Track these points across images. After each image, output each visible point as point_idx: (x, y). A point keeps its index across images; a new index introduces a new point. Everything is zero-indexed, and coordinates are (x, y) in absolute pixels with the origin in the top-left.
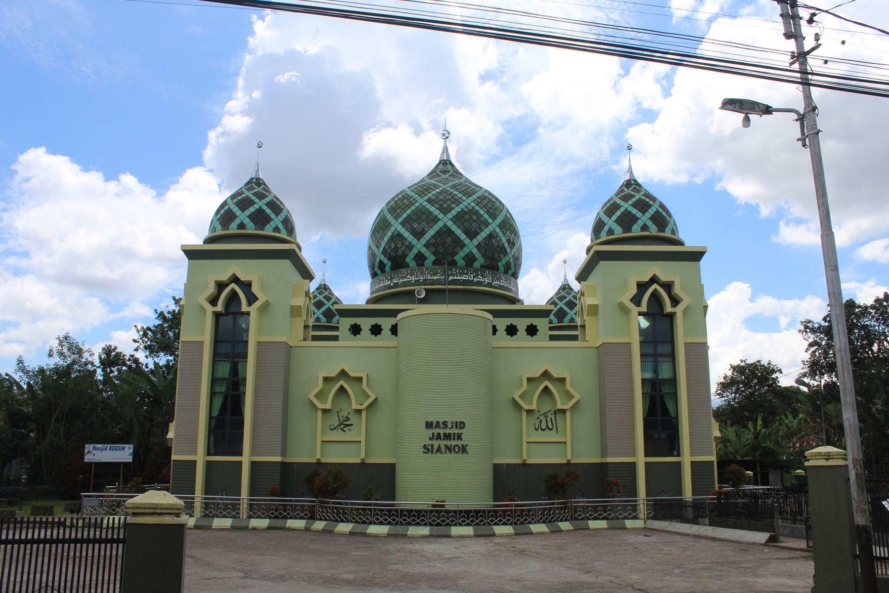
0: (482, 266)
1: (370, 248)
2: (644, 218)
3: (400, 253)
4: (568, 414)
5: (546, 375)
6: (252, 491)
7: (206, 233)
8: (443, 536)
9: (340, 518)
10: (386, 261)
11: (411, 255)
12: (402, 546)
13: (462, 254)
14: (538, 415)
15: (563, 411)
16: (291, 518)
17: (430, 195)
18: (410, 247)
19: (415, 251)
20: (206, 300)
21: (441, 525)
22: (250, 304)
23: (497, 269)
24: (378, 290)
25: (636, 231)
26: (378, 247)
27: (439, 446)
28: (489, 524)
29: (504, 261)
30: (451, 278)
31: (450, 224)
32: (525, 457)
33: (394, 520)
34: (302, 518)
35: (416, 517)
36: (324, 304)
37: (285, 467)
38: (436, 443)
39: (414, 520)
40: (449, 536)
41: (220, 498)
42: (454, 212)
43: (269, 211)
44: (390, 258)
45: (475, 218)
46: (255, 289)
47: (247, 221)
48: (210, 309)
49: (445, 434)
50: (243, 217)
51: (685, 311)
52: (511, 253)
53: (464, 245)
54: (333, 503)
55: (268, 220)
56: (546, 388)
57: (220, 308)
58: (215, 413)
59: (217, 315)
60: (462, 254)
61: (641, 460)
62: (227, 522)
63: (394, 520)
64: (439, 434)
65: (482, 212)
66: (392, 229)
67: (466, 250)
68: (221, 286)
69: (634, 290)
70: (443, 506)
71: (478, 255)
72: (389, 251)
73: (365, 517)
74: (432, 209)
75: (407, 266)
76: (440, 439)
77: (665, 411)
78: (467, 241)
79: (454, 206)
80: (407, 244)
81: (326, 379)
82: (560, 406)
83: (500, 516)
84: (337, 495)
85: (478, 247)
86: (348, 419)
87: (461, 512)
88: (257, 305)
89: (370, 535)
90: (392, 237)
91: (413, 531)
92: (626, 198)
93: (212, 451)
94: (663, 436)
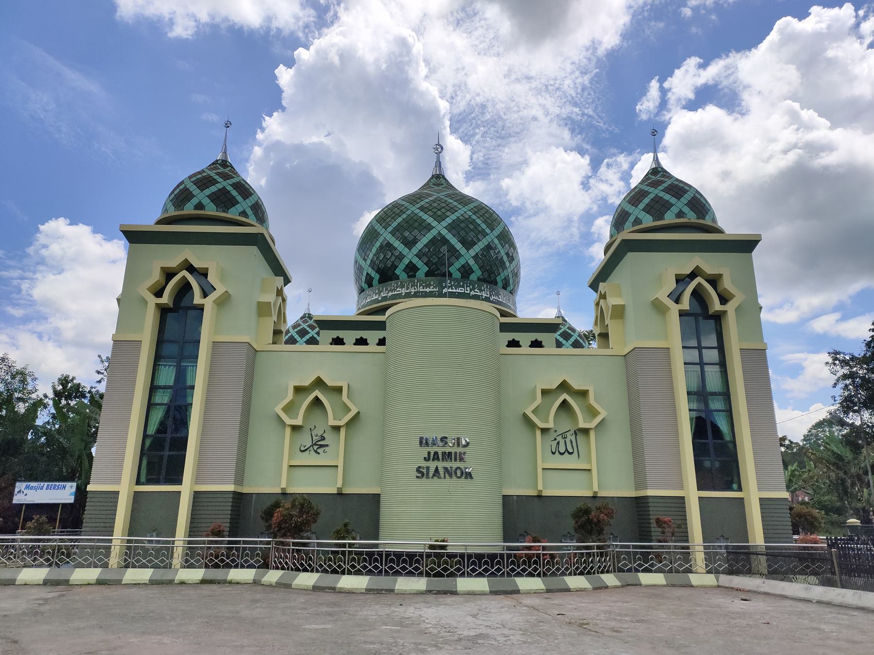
0: (479, 279)
1: (356, 262)
2: (679, 204)
3: (389, 264)
4: (592, 434)
5: (564, 386)
6: (193, 530)
7: (158, 215)
8: (445, 593)
9: (302, 565)
10: (373, 274)
11: (402, 266)
12: (387, 610)
13: (458, 265)
14: (554, 435)
15: (586, 431)
16: (236, 567)
17: (422, 203)
18: (401, 257)
19: (406, 261)
20: (149, 289)
21: (442, 576)
22: (205, 295)
23: (496, 283)
24: (364, 306)
25: (670, 218)
26: (365, 260)
27: (437, 468)
28: (509, 575)
29: (502, 276)
30: (445, 290)
31: (444, 232)
32: (540, 487)
33: (376, 567)
34: (251, 566)
35: (405, 563)
36: (308, 333)
37: (239, 499)
38: (432, 465)
39: (404, 568)
40: (454, 593)
41: (148, 540)
42: (449, 220)
43: (234, 193)
44: (378, 271)
45: (472, 227)
46: (212, 278)
47: (206, 201)
48: (153, 300)
49: (444, 454)
50: (201, 196)
51: (738, 310)
52: (510, 267)
53: (460, 255)
54: (294, 544)
55: (233, 202)
56: (565, 402)
57: (166, 299)
58: (152, 430)
59: (163, 311)
60: (458, 265)
61: (692, 494)
62: (92, 574)
63: (376, 567)
64: (436, 453)
65: (479, 221)
66: (381, 239)
67: (462, 261)
68: (169, 274)
69: (672, 285)
70: (443, 547)
71: (475, 267)
72: (377, 262)
73: (336, 565)
74: (425, 217)
75: (397, 278)
76: (438, 459)
77: (717, 432)
78: (463, 251)
79: (448, 213)
80: (397, 254)
81: (298, 390)
82: (582, 425)
83: (524, 562)
84: (302, 534)
85: (475, 257)
86: (323, 438)
87: (470, 556)
88: (213, 296)
89: (341, 591)
90: (381, 247)
91: (404, 583)
92: (655, 184)
93: (143, 479)
94: (717, 464)
